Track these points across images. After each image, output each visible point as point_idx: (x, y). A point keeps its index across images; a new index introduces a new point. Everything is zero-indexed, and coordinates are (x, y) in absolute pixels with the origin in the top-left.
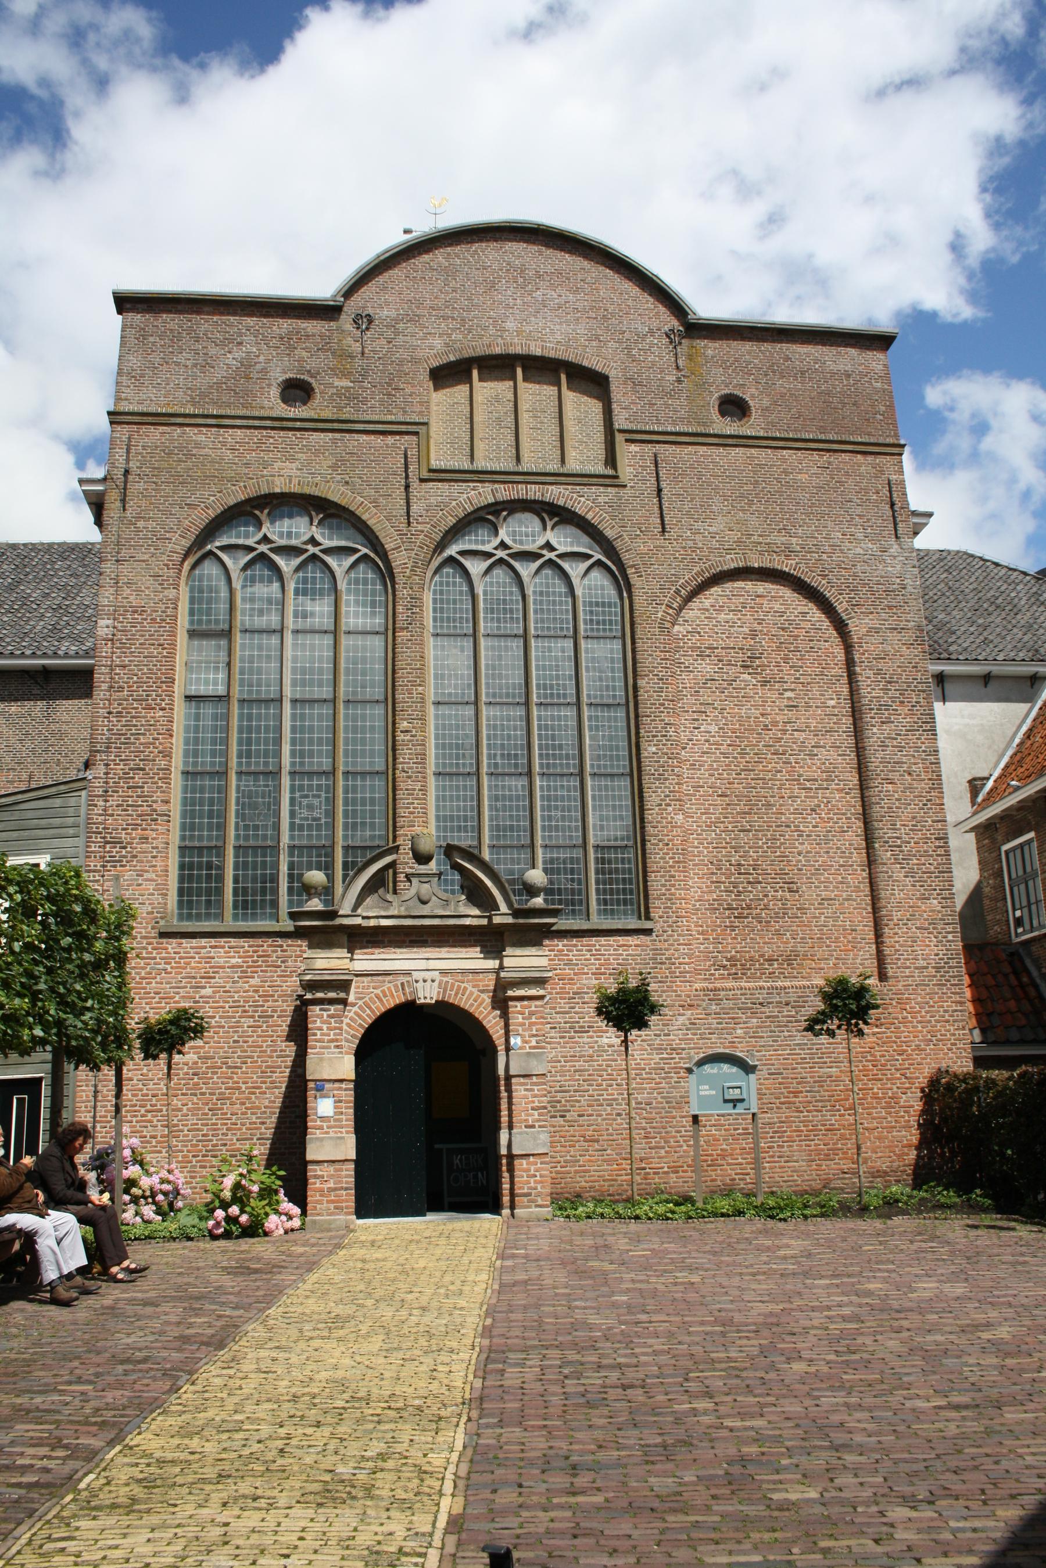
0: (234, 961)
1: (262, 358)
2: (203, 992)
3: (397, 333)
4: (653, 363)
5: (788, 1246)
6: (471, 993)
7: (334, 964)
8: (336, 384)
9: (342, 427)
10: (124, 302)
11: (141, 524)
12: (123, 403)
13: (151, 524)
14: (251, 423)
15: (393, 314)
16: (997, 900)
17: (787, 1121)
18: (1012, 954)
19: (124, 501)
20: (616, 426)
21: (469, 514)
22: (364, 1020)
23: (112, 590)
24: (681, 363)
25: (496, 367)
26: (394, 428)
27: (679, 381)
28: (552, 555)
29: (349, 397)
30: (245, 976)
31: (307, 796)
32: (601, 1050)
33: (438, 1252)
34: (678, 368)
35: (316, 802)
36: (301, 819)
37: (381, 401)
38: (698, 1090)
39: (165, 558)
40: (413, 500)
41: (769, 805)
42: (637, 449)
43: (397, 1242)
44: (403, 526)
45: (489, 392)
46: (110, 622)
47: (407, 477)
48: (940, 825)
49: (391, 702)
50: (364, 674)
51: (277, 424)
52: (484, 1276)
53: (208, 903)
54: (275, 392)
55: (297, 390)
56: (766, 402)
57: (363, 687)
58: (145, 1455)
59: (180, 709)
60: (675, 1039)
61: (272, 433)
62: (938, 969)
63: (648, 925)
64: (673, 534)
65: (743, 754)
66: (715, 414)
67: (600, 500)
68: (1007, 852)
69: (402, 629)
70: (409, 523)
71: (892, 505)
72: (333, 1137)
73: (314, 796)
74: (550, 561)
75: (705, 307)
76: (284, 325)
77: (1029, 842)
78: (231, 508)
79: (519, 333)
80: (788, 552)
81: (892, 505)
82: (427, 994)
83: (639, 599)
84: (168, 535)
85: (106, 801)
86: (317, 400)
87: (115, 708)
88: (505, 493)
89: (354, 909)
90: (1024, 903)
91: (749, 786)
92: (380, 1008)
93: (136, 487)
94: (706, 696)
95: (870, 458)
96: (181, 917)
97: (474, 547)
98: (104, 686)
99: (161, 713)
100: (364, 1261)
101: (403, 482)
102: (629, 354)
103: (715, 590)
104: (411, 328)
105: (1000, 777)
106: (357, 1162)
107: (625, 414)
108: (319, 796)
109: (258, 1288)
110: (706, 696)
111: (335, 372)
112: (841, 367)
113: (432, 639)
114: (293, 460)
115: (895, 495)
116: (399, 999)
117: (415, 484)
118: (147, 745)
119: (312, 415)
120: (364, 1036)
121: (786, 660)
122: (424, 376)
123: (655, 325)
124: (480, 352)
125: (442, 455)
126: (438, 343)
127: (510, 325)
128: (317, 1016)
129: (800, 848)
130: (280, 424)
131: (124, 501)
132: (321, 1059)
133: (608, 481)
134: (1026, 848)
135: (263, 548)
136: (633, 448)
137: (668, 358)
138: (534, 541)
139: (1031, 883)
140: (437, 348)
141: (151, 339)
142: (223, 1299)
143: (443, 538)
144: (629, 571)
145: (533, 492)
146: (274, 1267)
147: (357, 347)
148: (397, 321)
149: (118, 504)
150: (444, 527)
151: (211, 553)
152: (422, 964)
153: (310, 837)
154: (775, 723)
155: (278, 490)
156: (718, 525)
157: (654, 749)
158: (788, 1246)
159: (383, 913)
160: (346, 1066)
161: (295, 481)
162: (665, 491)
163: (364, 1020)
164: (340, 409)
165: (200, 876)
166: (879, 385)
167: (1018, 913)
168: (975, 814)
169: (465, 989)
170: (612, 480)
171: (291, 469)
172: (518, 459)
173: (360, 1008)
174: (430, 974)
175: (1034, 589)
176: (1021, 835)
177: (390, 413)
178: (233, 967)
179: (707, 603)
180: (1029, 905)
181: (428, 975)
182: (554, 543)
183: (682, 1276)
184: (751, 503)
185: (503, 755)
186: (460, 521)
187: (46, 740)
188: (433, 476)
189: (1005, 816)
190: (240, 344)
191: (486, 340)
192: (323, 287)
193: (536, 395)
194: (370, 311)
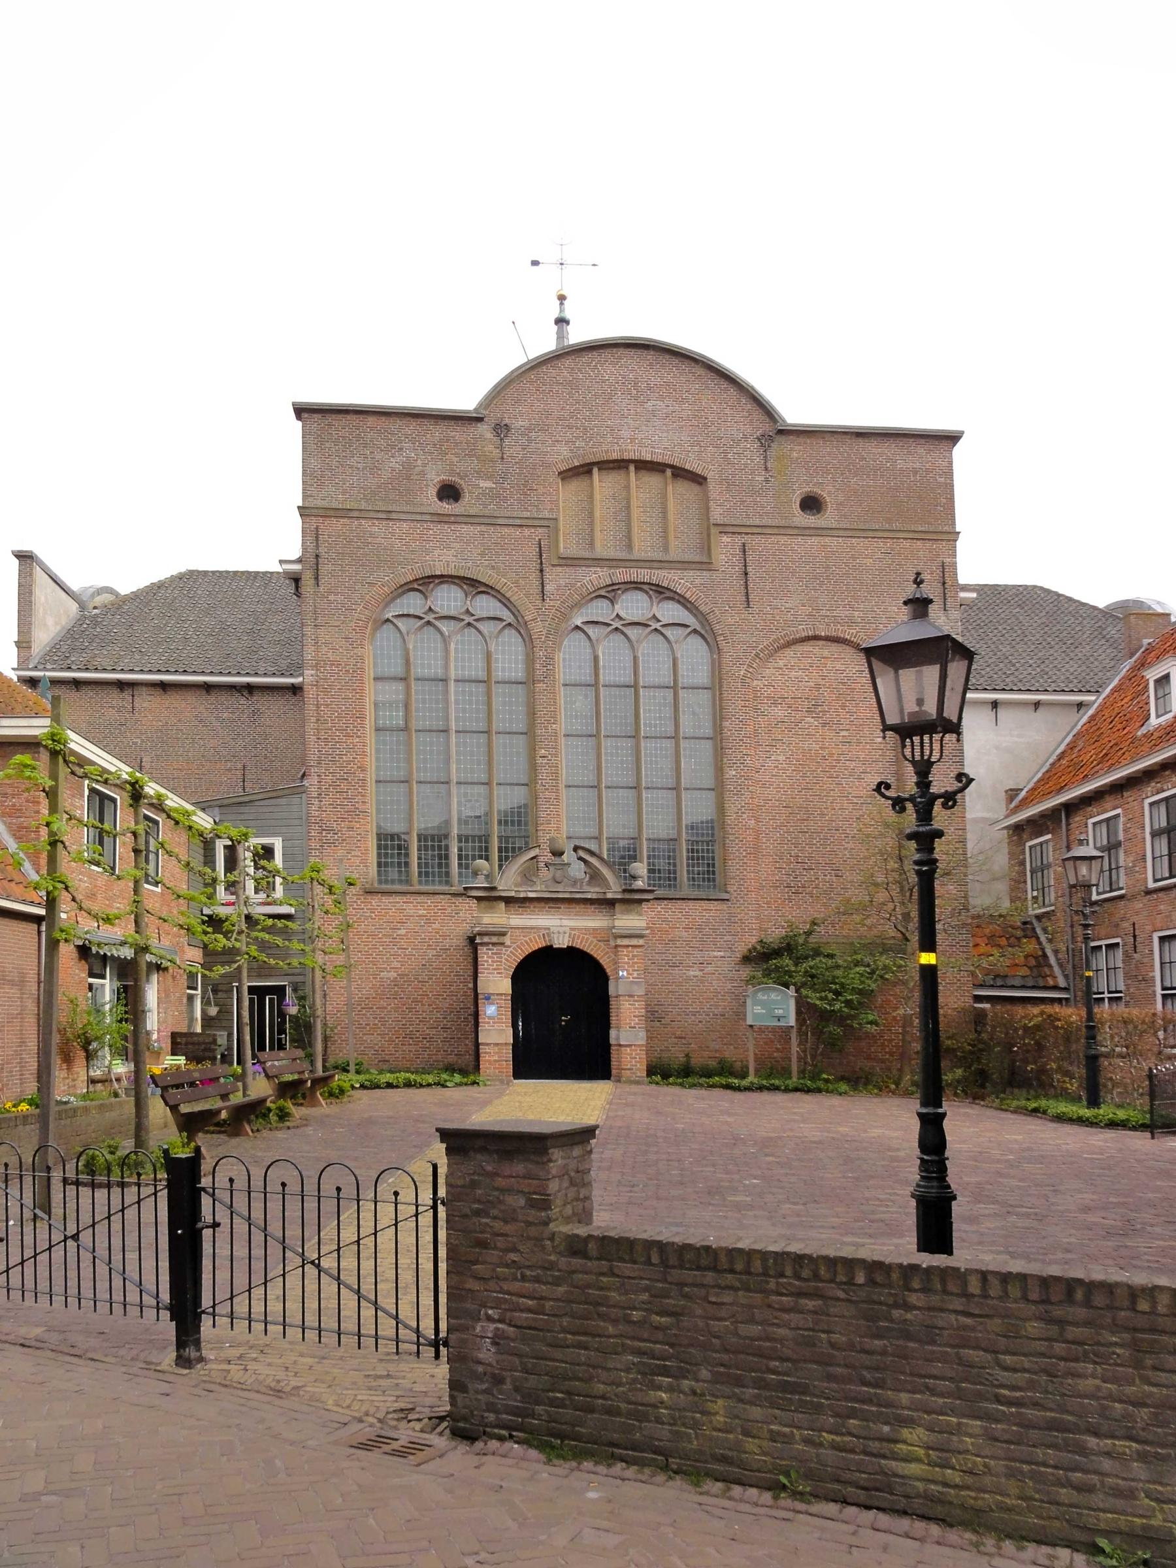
0: (421, 912)
1: (419, 463)
2: (400, 932)
4: (746, 465)
7: (496, 921)
9: (490, 521)
10: (301, 411)
11: (332, 597)
12: (310, 499)
13: (340, 598)
15: (526, 423)
16: (1019, 882)
18: (1025, 923)
19: (317, 579)
20: (712, 521)
24: (769, 465)
25: (613, 469)
26: (530, 523)
27: (767, 481)
28: (657, 626)
32: (689, 979)
34: (766, 469)
35: (477, 805)
37: (519, 499)
40: (546, 581)
42: (729, 540)
44: (539, 603)
45: (603, 485)
47: (541, 563)
48: (960, 832)
49: (530, 733)
54: (432, 492)
55: (449, 492)
56: (841, 498)
59: (370, 737)
63: (725, 896)
64: (755, 608)
68: (1031, 847)
69: (540, 681)
71: (944, 583)
72: (497, 1029)
75: (793, 413)
76: (437, 432)
77: (1046, 842)
79: (632, 440)
82: (561, 942)
83: (727, 658)
86: (466, 498)
87: (323, 735)
88: (620, 575)
89: (508, 882)
90: (1040, 886)
91: (807, 800)
92: (528, 950)
93: (323, 569)
95: (928, 544)
96: (380, 882)
98: (313, 719)
101: (538, 567)
102: (725, 458)
103: (789, 652)
106: (513, 1045)
107: (719, 510)
111: (480, 474)
113: (562, 688)
114: (449, 548)
116: (541, 944)
118: (349, 762)
121: (843, 707)
122: (553, 478)
125: (568, 546)
127: (625, 433)
130: (441, 519)
131: (317, 579)
134: (1044, 846)
135: (430, 617)
136: (725, 539)
137: (758, 459)
139: (1045, 872)
140: (563, 455)
144: (720, 638)
145: (644, 575)
148: (529, 429)
149: (313, 581)
151: (388, 620)
152: (558, 922)
154: (831, 755)
155: (438, 573)
160: (505, 985)
162: (750, 575)
164: (485, 506)
165: (392, 854)
167: (1035, 893)
168: (1007, 817)
170: (706, 565)
172: (630, 547)
174: (562, 928)
175: (1100, 623)
176: (1041, 835)
179: (781, 663)
180: (1043, 888)
181: (561, 930)
182: (659, 616)
184: (822, 584)
189: (1030, 821)
190: (401, 449)
191: (604, 447)
192: (467, 402)
193: (644, 488)
194: (507, 421)
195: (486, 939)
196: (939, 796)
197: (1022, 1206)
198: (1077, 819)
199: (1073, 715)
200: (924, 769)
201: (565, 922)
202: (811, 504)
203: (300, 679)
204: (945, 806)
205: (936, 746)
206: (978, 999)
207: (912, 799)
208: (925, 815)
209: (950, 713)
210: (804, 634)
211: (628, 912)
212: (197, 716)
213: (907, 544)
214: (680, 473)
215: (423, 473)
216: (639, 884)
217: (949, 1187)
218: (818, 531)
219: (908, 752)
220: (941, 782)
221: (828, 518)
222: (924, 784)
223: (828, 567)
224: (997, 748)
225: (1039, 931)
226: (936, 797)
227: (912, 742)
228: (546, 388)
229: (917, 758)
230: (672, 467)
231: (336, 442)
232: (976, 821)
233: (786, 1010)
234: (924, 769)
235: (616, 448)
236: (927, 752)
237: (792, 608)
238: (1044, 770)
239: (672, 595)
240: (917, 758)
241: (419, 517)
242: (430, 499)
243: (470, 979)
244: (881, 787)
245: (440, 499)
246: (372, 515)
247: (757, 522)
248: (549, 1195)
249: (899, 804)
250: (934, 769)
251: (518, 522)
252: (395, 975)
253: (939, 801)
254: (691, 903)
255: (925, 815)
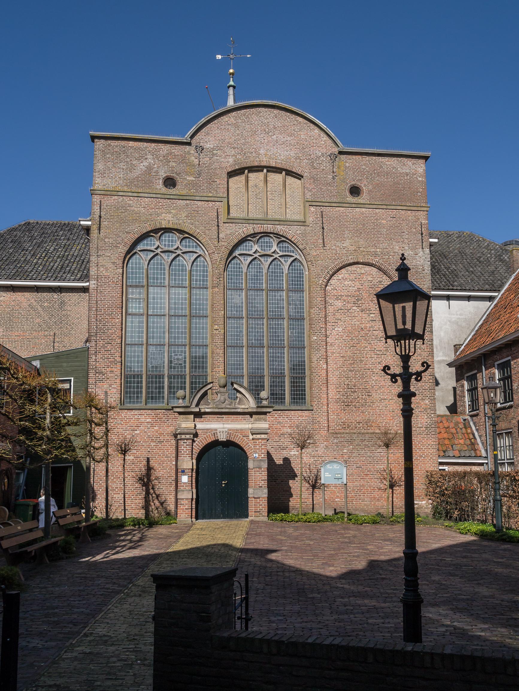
0: (148, 420)
1: (156, 166)
2: (136, 432)
3: (213, 155)
5: (349, 533)
6: (240, 437)
8: (188, 178)
11: (107, 240)
13: (111, 241)
14: (152, 195)
17: (363, 486)
21: (243, 238)
22: (199, 447)
23: (96, 269)
26: (212, 199)
29: (193, 184)
30: (152, 426)
31: (177, 355)
33: (225, 532)
35: (180, 357)
36: (175, 364)
37: (207, 187)
38: (324, 475)
39: (117, 255)
41: (361, 361)
42: (314, 209)
43: (210, 528)
44: (216, 243)
46: (95, 282)
50: (200, 305)
51: (163, 196)
52: (240, 541)
53: (137, 397)
55: (170, 182)
57: (199, 310)
58: (139, 586)
60: (320, 453)
61: (161, 200)
62: (426, 428)
65: (352, 340)
66: (348, 194)
67: (298, 232)
70: (219, 242)
71: (422, 234)
73: (180, 355)
74: (276, 258)
78: (144, 234)
80: (375, 255)
81: (422, 234)
82: (222, 438)
84: (118, 245)
85: (96, 356)
88: (258, 228)
93: (104, 223)
94: (338, 316)
95: (414, 213)
97: (245, 252)
99: (117, 320)
100: (199, 535)
101: (216, 223)
104: (219, 153)
105: (467, 345)
108: (182, 355)
109: (163, 544)
110: (338, 316)
112: (404, 171)
114: (170, 213)
115: (423, 230)
116: (213, 439)
117: (221, 224)
119: (177, 192)
120: (199, 452)
123: (324, 151)
124: (249, 165)
126: (231, 160)
127: (262, 151)
128: (182, 445)
129: (373, 378)
130: (165, 197)
132: (183, 461)
133: (301, 224)
136: (312, 209)
137: (329, 167)
138: (270, 250)
141: (108, 156)
142: (152, 547)
143: (232, 248)
146: (167, 536)
147: (196, 161)
148: (213, 149)
149: (97, 231)
150: (233, 244)
152: (221, 426)
153: (178, 371)
154: (366, 327)
155: (163, 226)
156: (347, 243)
157: (316, 338)
158: (349, 533)
159: (207, 407)
161: (171, 222)
163: (199, 447)
165: (134, 386)
166: (420, 179)
169: (238, 435)
171: (169, 217)
173: (198, 442)
176: (472, 371)
177: (210, 192)
178: (148, 422)
179: (340, 277)
181: (224, 430)
183: (308, 542)
185: (255, 339)
186: (239, 241)
187: (61, 318)
188: (229, 221)
194: (202, 144)
195: (183, 437)
196: (414, 374)
197: (462, 595)
198: (490, 362)
199: (488, 304)
200: (406, 359)
201: (226, 426)
202: (355, 191)
203: (88, 284)
204: (416, 379)
205: (412, 346)
206: (441, 464)
207: (400, 375)
208: (406, 384)
209: (418, 330)
210: (352, 261)
211: (259, 420)
212: (30, 305)
213: (403, 212)
214: (289, 173)
215: (157, 172)
216: (265, 403)
217: (419, 595)
218: (358, 205)
219: (398, 350)
220: (415, 366)
221: (363, 199)
222: (406, 367)
223: (364, 225)
224: (450, 321)
225: (472, 424)
226: (413, 374)
227: (401, 343)
228: (223, 127)
229: (403, 353)
230: (286, 170)
231: (112, 154)
232: (440, 362)
233: (342, 474)
234: (406, 359)
235: (257, 159)
236: (407, 352)
237: (345, 246)
238: (473, 334)
239: (285, 239)
240: (403, 353)
241: (154, 196)
242: (160, 186)
243: (174, 459)
244: (386, 369)
245: (166, 186)
246: (130, 194)
247: (329, 200)
248: (210, 613)
249: (394, 378)
250: (412, 360)
251: (206, 199)
252: (133, 458)
253: (414, 377)
254: (292, 412)
255: (406, 384)
